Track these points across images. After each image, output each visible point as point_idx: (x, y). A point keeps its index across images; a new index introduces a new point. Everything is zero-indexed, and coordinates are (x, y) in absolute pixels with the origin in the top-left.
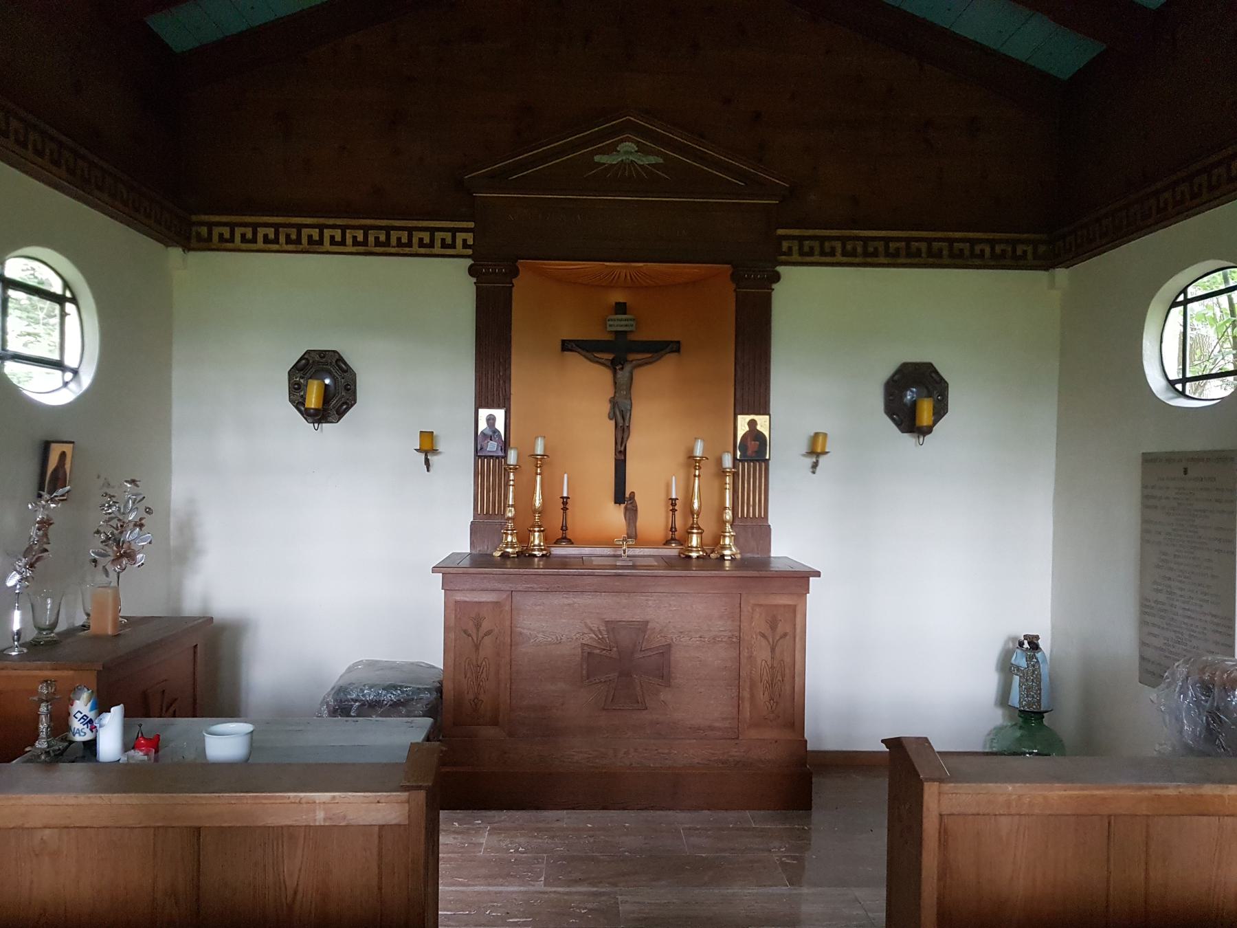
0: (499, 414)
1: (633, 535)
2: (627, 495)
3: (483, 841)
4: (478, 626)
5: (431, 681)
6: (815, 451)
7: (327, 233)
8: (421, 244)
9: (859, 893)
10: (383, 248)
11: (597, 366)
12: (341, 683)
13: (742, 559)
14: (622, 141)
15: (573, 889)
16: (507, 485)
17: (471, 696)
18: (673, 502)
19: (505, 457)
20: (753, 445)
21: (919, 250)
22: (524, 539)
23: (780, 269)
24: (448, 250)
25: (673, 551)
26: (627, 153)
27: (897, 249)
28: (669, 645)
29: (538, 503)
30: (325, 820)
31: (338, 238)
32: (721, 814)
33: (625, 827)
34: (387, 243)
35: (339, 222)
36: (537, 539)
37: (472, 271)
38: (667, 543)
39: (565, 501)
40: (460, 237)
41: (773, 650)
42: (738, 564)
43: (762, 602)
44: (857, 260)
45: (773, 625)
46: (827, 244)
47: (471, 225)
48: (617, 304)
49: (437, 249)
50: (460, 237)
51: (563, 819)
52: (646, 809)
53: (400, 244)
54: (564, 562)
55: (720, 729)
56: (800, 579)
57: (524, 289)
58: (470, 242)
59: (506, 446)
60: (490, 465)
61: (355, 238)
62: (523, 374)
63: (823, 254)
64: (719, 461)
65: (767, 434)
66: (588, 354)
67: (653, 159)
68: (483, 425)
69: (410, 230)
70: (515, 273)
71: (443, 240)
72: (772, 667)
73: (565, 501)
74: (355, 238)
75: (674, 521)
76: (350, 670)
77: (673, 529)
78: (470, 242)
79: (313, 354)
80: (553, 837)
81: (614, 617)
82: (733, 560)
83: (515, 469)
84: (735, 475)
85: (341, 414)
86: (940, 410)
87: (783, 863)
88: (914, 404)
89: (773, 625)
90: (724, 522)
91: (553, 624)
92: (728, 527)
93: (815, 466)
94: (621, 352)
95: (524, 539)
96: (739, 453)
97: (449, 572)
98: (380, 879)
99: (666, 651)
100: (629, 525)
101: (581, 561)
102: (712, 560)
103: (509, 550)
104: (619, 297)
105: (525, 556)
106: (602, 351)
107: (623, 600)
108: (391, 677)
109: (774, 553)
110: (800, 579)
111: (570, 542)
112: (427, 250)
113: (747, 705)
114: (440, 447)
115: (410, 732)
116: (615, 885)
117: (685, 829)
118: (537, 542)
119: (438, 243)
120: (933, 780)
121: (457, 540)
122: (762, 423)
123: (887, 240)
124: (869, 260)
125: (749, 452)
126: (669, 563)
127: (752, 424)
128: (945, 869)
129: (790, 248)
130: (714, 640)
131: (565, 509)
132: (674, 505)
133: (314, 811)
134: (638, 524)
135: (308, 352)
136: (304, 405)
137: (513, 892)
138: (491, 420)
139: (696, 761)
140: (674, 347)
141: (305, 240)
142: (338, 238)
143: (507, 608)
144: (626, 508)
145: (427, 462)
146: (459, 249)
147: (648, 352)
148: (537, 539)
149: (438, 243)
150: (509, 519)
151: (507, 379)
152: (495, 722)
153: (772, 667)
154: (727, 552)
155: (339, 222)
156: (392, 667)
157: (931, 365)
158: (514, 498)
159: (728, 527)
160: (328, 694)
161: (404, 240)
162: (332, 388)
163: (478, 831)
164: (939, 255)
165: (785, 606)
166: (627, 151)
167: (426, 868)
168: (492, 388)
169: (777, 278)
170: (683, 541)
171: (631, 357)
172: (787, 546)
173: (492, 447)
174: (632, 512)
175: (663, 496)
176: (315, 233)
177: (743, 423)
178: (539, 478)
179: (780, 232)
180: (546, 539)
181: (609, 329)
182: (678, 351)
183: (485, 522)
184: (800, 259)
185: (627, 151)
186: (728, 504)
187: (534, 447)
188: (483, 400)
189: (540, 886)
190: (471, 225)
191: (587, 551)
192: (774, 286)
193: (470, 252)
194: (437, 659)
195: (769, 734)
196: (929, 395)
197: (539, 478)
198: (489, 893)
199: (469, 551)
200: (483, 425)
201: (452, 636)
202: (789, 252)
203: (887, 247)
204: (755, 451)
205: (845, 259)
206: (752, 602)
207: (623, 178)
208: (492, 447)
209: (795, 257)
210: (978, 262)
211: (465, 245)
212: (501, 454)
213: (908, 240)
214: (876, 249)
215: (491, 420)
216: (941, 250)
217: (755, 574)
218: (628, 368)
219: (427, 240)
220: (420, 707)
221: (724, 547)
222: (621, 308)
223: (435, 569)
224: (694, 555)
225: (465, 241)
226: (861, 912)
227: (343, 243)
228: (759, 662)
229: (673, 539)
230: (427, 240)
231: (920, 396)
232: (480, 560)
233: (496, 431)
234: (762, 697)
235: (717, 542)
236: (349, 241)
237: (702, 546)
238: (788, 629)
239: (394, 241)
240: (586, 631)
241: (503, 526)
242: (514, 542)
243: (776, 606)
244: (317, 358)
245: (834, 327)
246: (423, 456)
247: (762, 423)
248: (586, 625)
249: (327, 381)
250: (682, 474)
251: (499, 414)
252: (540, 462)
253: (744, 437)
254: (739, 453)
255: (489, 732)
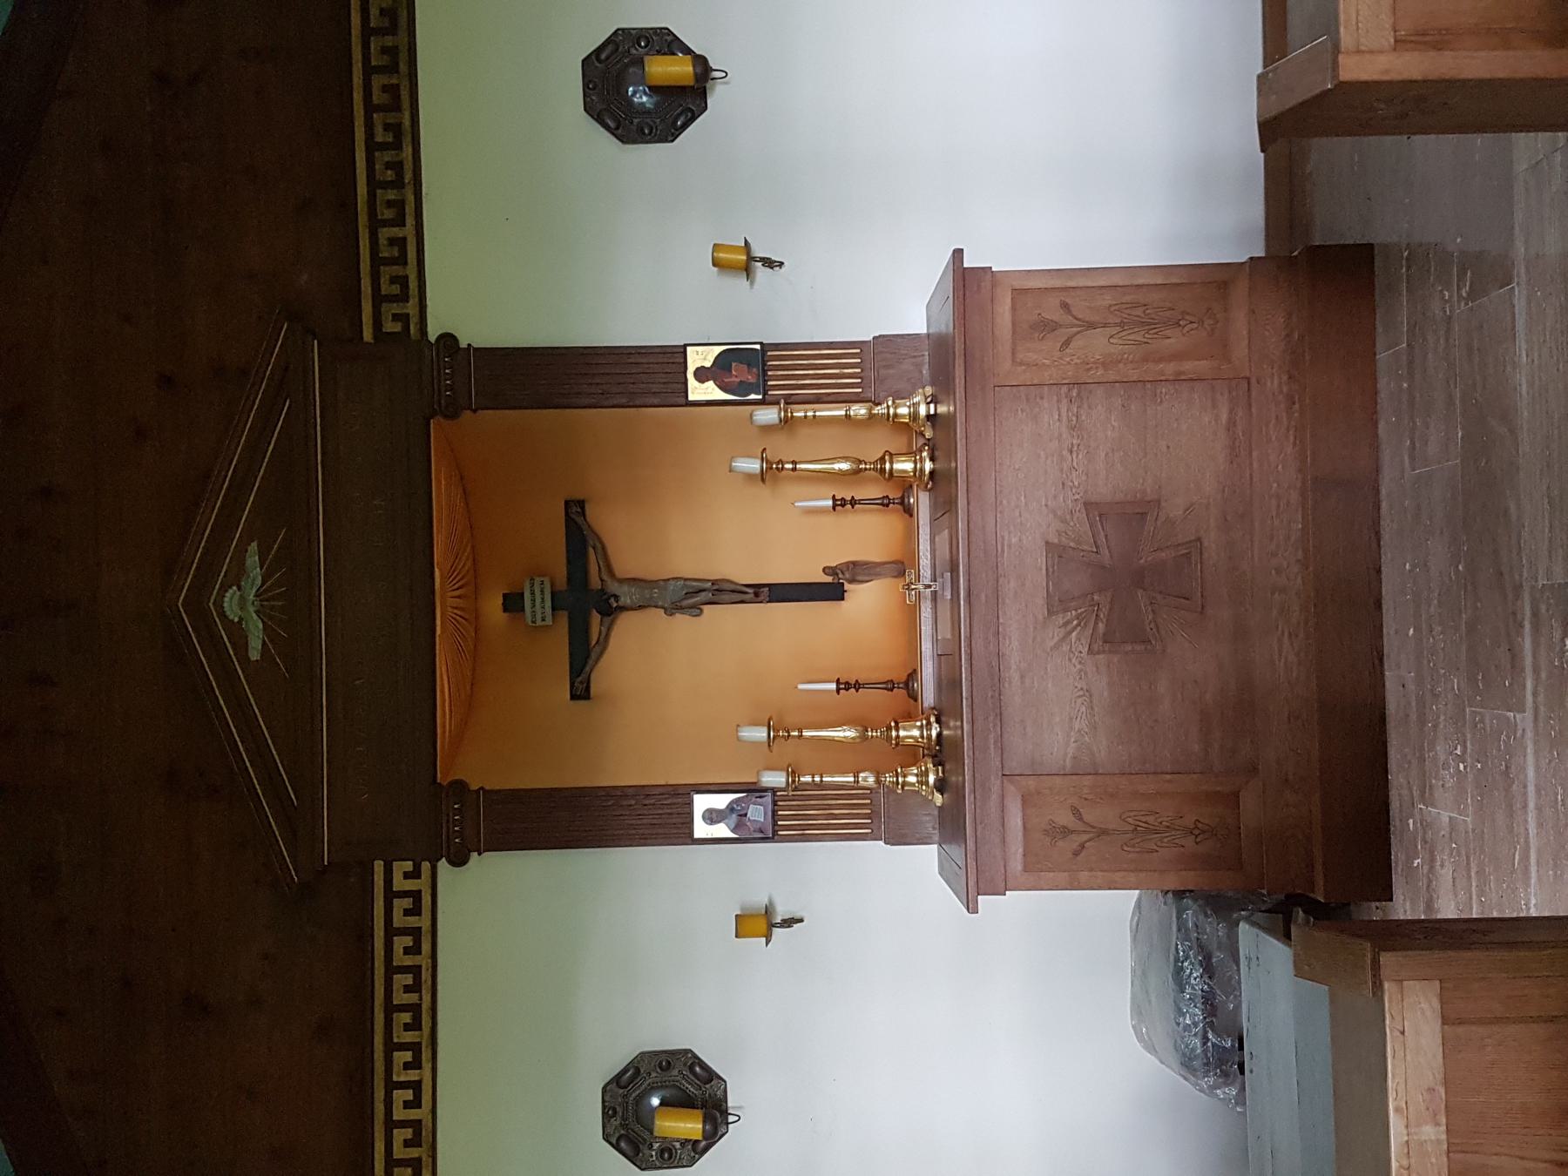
0: (702, 803)
1: (901, 567)
2: (829, 579)
3: (1445, 817)
4: (1066, 832)
5: (1164, 909)
6: (744, 263)
7: (399, 1114)
8: (414, 950)
9: (1521, 166)
10: (423, 1017)
11: (612, 641)
12: (1176, 1065)
13: (933, 384)
14: (222, 615)
15: (1528, 661)
16: (822, 786)
17: (1189, 842)
18: (839, 504)
19: (774, 791)
20: (739, 373)
21: (385, 88)
22: (910, 754)
23: (432, 338)
24: (422, 903)
25: (922, 502)
26: (242, 606)
27: (387, 127)
28: (1088, 505)
29: (849, 733)
30: (1438, 1124)
31: (409, 1095)
32: (1383, 396)
33: (1413, 572)
34: (415, 1009)
35: (380, 1094)
36: (910, 733)
37: (459, 861)
38: (908, 511)
39: (844, 686)
40: (399, 883)
41: (1092, 326)
42: (943, 386)
43: (1008, 346)
44: (411, 198)
45: (1046, 327)
46: (384, 254)
47: (379, 866)
48: (505, 610)
49: (424, 922)
50: (399, 883)
51: (1400, 684)
52: (1378, 534)
53: (415, 988)
54: (949, 684)
55: (1231, 411)
56: (967, 284)
57: (483, 767)
58: (408, 866)
59: (754, 790)
60: (785, 816)
61: (407, 1066)
62: (627, 766)
63: (402, 260)
64: (767, 429)
65: (718, 350)
66: (593, 656)
67: (252, 559)
68: (722, 830)
69: (391, 970)
70: (460, 786)
71: (407, 912)
72: (1121, 324)
73: (844, 686)
74: (407, 1066)
75: (871, 502)
76: (1151, 1049)
77: (885, 503)
78: (408, 866)
79: (608, 1130)
80: (1436, 696)
81: (1040, 601)
82: (934, 400)
83: (794, 773)
84: (790, 400)
85: (711, 1076)
86: (667, 42)
87: (1472, 295)
88: (654, 90)
89: (1046, 327)
90: (871, 416)
91: (1058, 702)
92: (878, 410)
93: (769, 263)
94: (587, 600)
95: (910, 754)
96: (753, 396)
97: (977, 882)
98: (1533, 1020)
99: (1095, 509)
100: (878, 575)
101: (947, 658)
102: (937, 435)
103: (932, 779)
104: (493, 607)
105: (941, 752)
106: (587, 631)
107: (1010, 586)
108: (1161, 978)
109: (916, 323)
110: (967, 284)
111: (913, 675)
112: (424, 940)
113: (1188, 366)
114: (761, 900)
115: (1269, 971)
116: (1518, 588)
117: (1414, 463)
118: (916, 733)
119: (412, 921)
120: (1335, 63)
121: (922, 863)
122: (699, 358)
123: (372, 147)
124: (408, 177)
125: (751, 379)
126: (945, 507)
127: (702, 374)
128: (1494, 35)
129: (396, 317)
130: (1075, 427)
131: (858, 686)
132: (843, 503)
133: (1422, 1144)
134: (878, 560)
135: (606, 1138)
136: (697, 1142)
137: (1537, 768)
138: (712, 817)
139: (1289, 450)
140: (575, 510)
141: (414, 1153)
142: (409, 1095)
143: (1031, 783)
144: (851, 581)
145: (788, 923)
146: (422, 884)
147: (585, 555)
148: (910, 733)
149: (412, 921)
150: (878, 781)
151: (642, 792)
152: (1233, 799)
153: (1121, 324)
154: (923, 411)
155: (380, 1094)
156: (1141, 974)
157: (586, 62)
158: (844, 773)
159: (878, 410)
160: (1195, 1085)
161: (408, 979)
162: (667, 1093)
163: (1425, 825)
164: (391, 52)
165: (1014, 309)
166: (241, 603)
167: (1511, 945)
168: (656, 817)
169: (448, 339)
170: (905, 485)
171: (595, 583)
172: (909, 308)
173: (757, 813)
174: (858, 571)
175: (830, 520)
176: (400, 1135)
177: (699, 391)
178: (806, 733)
179: (368, 335)
180: (909, 717)
181: (549, 621)
182: (581, 504)
183: (887, 821)
184: (413, 302)
185: (241, 603)
186: (840, 412)
187: (755, 744)
188: (681, 832)
189: (1524, 720)
190: (379, 866)
191: (927, 647)
192: (463, 344)
193: (426, 866)
194: (1124, 901)
195: (1240, 321)
196: (640, 62)
197: (806, 733)
198: (1539, 808)
199: (935, 846)
200: (722, 830)
201: (1084, 876)
202: (403, 318)
203: (384, 147)
204: (748, 367)
205: (410, 221)
206: (1007, 365)
207: (288, 602)
208: (757, 813)
209: (411, 308)
210: (403, 56)
211: (415, 874)
212: (768, 798)
213: (370, 108)
214: (388, 166)
215: (712, 817)
216: (384, 50)
217: (959, 363)
218: (613, 587)
219: (408, 941)
220: (1214, 930)
221: (914, 416)
222: (513, 603)
223: (972, 908)
224: (928, 466)
225: (407, 876)
226: (1558, 157)
227: (416, 1086)
228: (1112, 350)
229: (902, 503)
230: (408, 941)
231: (641, 80)
232: (951, 827)
233: (731, 808)
234: (1174, 340)
235: (906, 428)
236: (412, 1075)
237: (910, 453)
238: (1054, 301)
239: (411, 998)
240: (1065, 648)
241: (891, 791)
242: (917, 767)
243: (1014, 324)
244: (616, 1122)
245: (528, 239)
246: (775, 930)
247: (699, 358)
248: (1056, 647)
249: (655, 1101)
250: (791, 490)
251: (702, 803)
252: (779, 730)
253: (724, 388)
254: (753, 396)
255: (1251, 808)
